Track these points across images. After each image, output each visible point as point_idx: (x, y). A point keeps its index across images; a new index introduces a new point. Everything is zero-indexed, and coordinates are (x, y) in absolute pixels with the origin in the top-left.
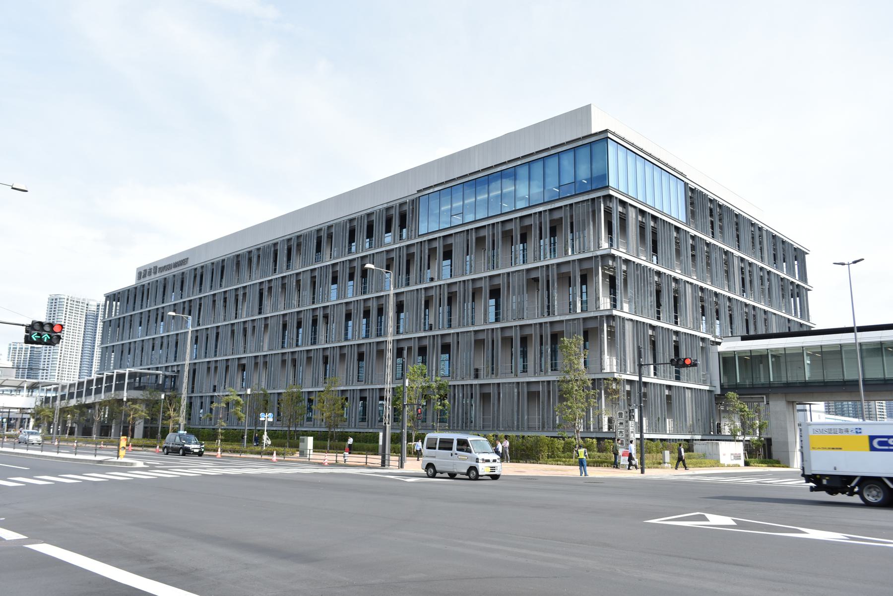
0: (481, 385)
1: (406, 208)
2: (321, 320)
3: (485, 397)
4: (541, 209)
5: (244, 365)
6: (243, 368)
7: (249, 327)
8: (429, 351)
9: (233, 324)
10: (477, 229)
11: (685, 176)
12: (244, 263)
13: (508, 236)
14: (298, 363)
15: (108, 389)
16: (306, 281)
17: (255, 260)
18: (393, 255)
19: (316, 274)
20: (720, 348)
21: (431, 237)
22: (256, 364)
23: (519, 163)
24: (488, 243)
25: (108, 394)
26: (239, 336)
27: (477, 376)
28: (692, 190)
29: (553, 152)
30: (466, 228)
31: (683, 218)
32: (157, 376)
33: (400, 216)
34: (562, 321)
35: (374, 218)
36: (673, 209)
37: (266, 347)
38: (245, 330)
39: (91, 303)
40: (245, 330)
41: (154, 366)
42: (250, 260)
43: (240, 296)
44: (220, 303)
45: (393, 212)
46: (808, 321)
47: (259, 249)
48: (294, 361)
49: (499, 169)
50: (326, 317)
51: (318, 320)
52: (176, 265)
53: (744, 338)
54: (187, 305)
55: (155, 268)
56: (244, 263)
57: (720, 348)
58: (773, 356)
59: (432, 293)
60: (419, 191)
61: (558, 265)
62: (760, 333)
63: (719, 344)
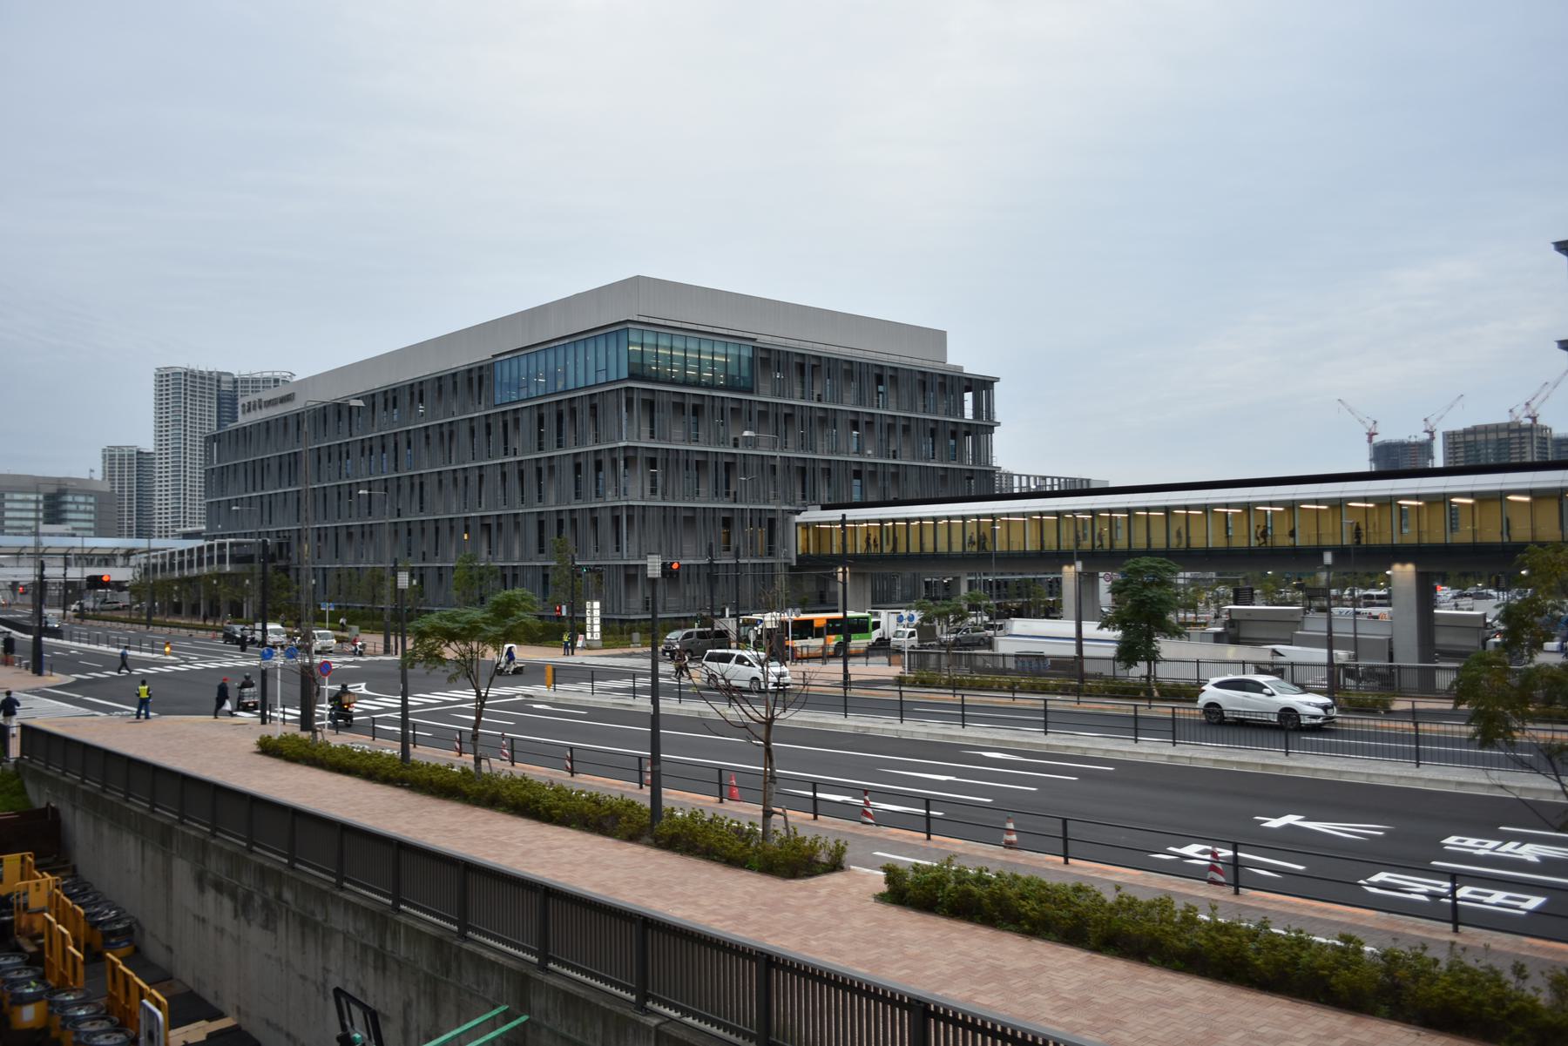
33: (476, 379)
39: (224, 378)
53: (825, 508)
57: (798, 519)
63: (798, 512)
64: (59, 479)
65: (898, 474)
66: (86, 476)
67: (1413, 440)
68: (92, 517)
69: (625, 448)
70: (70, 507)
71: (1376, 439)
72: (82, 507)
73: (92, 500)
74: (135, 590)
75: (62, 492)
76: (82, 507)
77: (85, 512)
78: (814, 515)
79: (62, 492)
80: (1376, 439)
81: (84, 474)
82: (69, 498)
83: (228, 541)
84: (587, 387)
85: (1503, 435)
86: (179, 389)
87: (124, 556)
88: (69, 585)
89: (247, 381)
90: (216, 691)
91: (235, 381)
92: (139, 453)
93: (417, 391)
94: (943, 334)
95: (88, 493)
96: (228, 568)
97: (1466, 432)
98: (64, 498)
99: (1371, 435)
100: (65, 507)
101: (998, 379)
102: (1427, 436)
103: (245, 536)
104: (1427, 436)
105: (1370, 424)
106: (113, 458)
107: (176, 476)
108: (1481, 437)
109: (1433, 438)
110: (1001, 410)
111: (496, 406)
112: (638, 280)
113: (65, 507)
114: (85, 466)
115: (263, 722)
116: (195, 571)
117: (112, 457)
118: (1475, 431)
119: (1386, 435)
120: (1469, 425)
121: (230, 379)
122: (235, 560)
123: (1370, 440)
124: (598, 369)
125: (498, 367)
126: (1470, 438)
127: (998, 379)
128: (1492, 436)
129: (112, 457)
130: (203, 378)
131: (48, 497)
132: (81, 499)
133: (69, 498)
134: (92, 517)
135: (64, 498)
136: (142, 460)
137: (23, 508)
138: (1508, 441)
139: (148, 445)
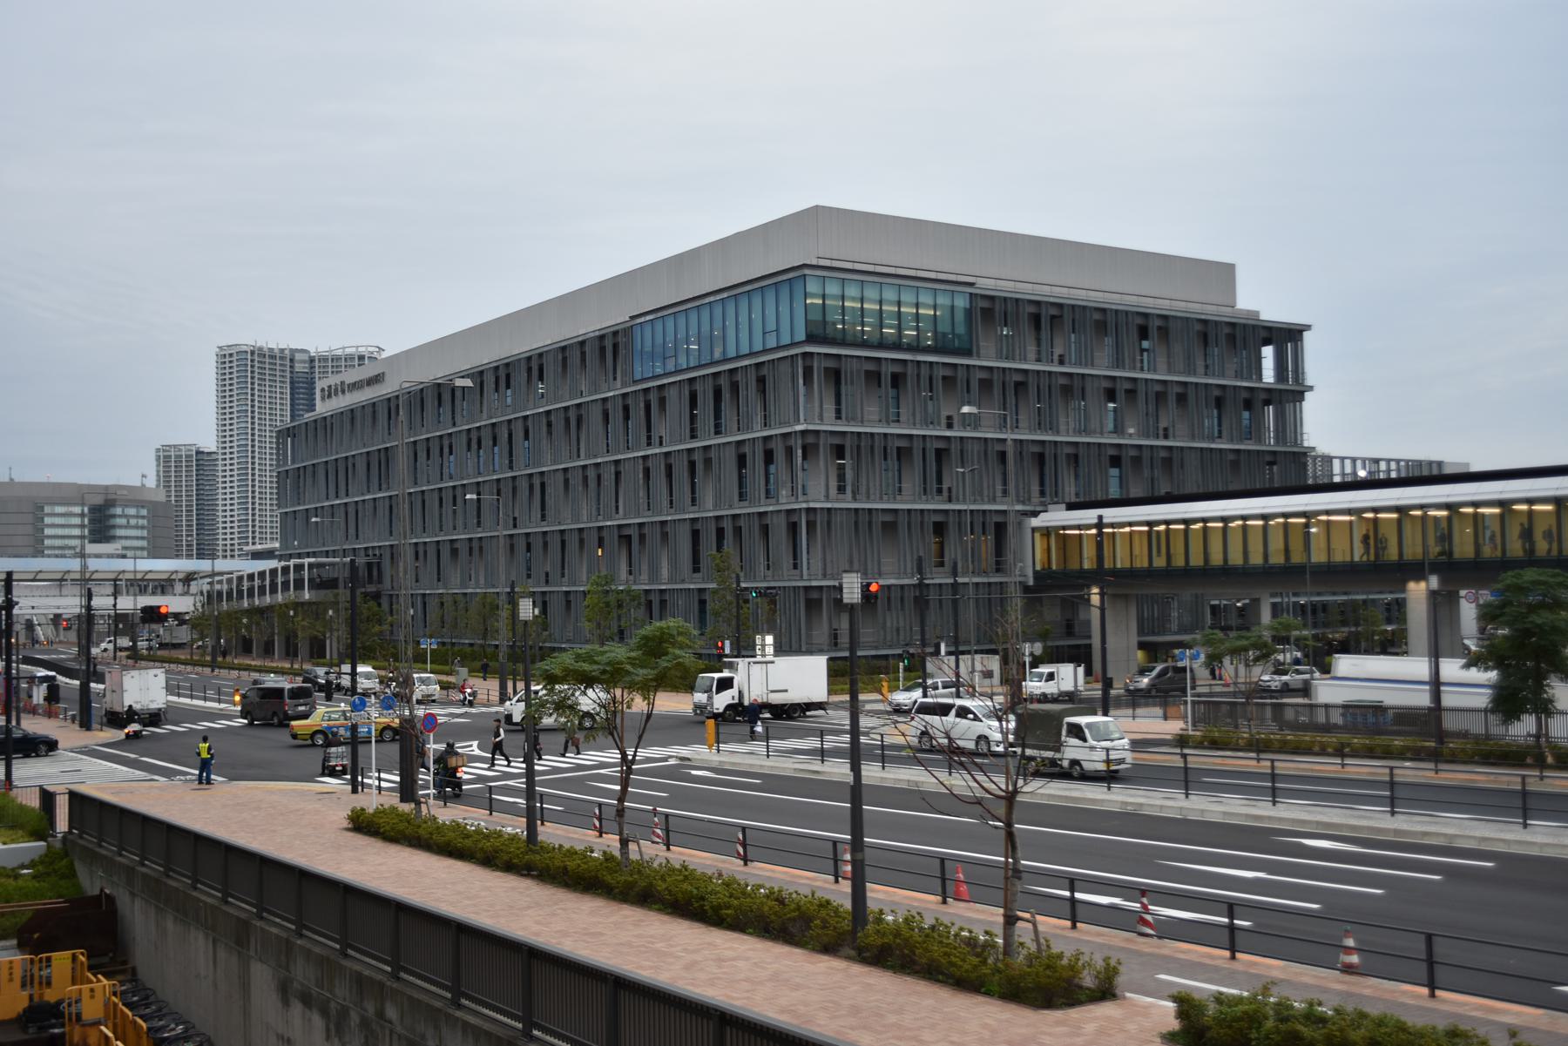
29: (756, 285)
33: (609, 349)
38: (692, 464)
39: (298, 356)
40: (692, 464)
49: (707, 300)
60: (632, 318)
63: (1035, 514)
69: (803, 432)
70: (120, 521)
72: (133, 522)
73: (144, 512)
76: (133, 522)
77: (137, 527)
78: (1057, 517)
82: (119, 511)
83: (306, 561)
84: (752, 354)
86: (245, 370)
91: (312, 360)
92: (198, 453)
95: (140, 504)
101: (1308, 327)
106: (169, 460)
111: (635, 382)
112: (817, 212)
117: (167, 458)
122: (314, 585)
124: (771, 329)
127: (1308, 327)
129: (167, 458)
131: (95, 510)
132: (132, 511)
133: (119, 511)
139: (209, 443)
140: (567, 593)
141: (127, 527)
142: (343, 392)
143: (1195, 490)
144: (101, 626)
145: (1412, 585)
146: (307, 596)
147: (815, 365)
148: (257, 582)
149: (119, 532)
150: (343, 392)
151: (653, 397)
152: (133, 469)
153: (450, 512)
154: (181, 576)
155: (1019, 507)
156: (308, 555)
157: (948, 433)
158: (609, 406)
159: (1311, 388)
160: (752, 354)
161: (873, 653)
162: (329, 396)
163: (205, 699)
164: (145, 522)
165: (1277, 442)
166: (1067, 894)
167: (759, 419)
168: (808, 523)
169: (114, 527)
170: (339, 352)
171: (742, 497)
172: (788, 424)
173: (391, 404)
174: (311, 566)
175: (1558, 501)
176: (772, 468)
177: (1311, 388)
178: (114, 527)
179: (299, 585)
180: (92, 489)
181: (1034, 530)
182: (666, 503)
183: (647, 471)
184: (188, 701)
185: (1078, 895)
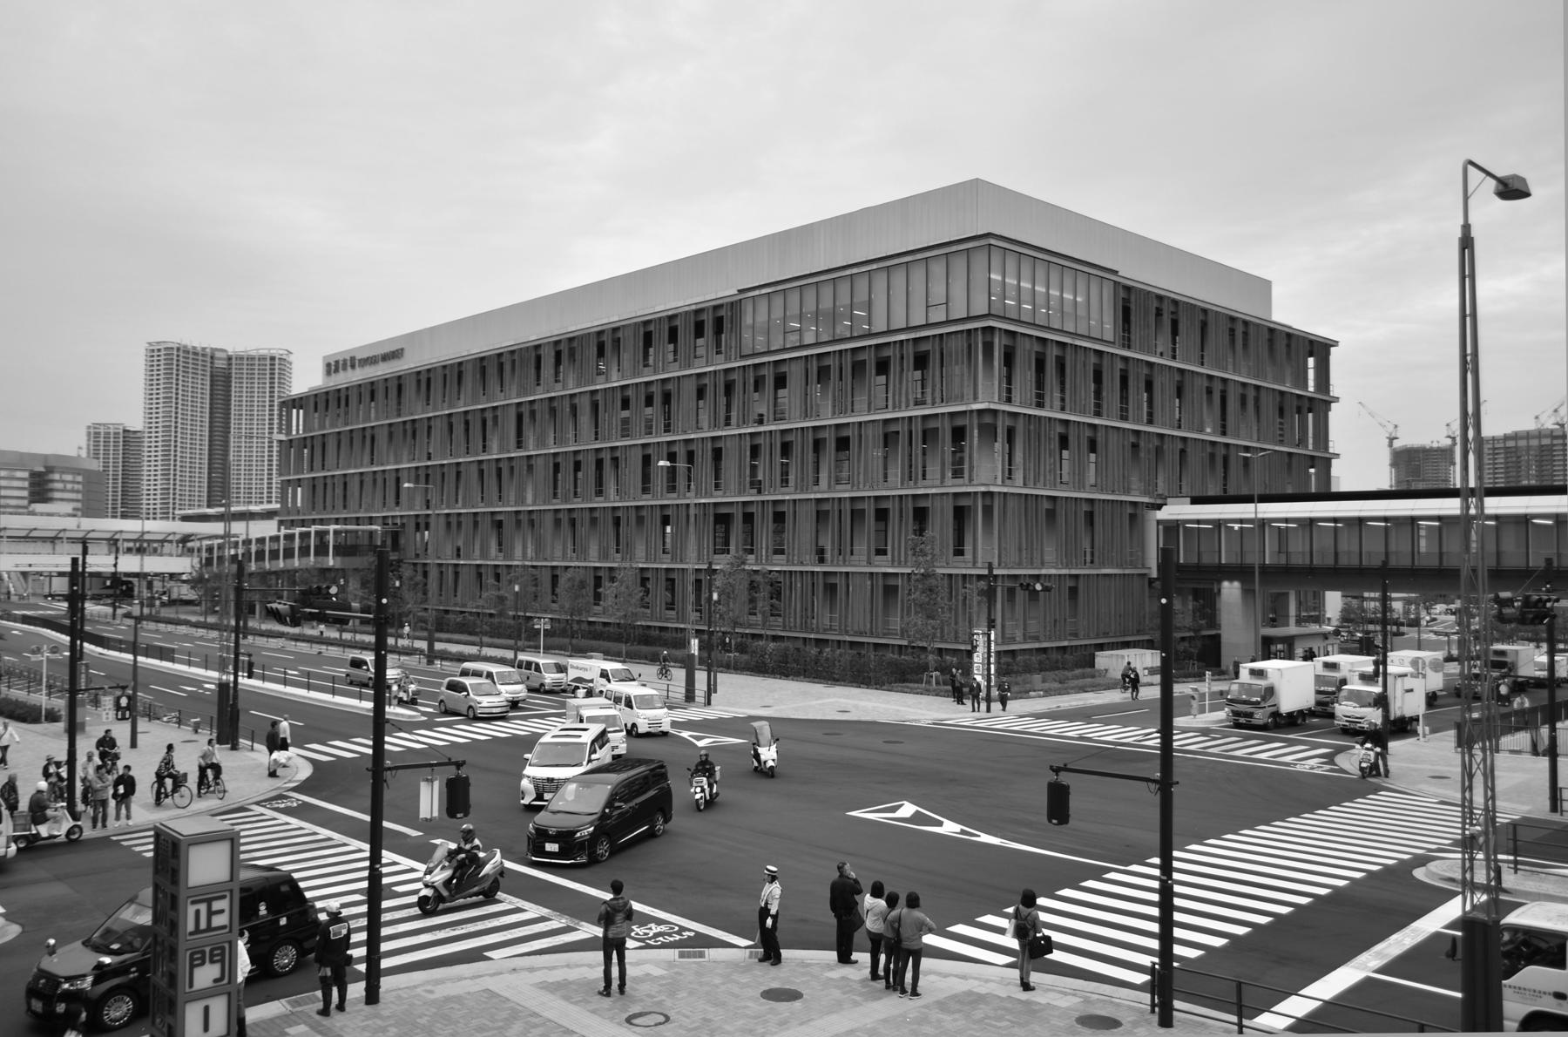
0: (825, 573)
1: (722, 313)
2: (607, 464)
3: (831, 589)
4: (903, 337)
5: (501, 522)
6: (499, 525)
7: (505, 467)
8: (757, 520)
9: (480, 462)
10: (819, 355)
11: (1115, 272)
12: (492, 371)
13: (858, 368)
14: (578, 523)
15: (304, 551)
16: (585, 405)
17: (507, 367)
18: (706, 381)
19: (599, 397)
20: (1162, 514)
21: (757, 361)
22: (518, 523)
23: (875, 266)
24: (834, 374)
25: (304, 560)
26: (491, 481)
27: (822, 561)
28: (1128, 289)
29: (919, 256)
30: (805, 353)
31: (1109, 330)
32: (371, 533)
33: (714, 322)
34: (927, 495)
35: (678, 322)
36: (1093, 322)
37: (529, 499)
38: (499, 471)
39: (218, 355)
40: (499, 471)
41: (372, 518)
42: (501, 366)
43: (485, 422)
44: (459, 429)
45: (704, 317)
46: (1326, 448)
47: (512, 352)
48: (573, 523)
49: (848, 272)
50: (615, 460)
51: (603, 466)
52: (386, 357)
53: (1196, 501)
54: (408, 426)
55: (353, 359)
56: (492, 371)
57: (1162, 514)
58: (975, 693)
59: (760, 441)
60: (740, 291)
61: (925, 417)
62: (1231, 492)
63: (1159, 507)
64: (46, 457)
65: (1220, 458)
66: (73, 453)
67: (1435, 445)
68: (80, 496)
69: (980, 412)
70: (59, 486)
71: (1397, 444)
72: (69, 486)
73: (79, 478)
74: (196, 582)
75: (50, 470)
76: (69, 486)
77: (72, 491)
78: (1179, 510)
79: (50, 470)
80: (1397, 444)
81: (71, 452)
82: (57, 476)
83: (332, 527)
84: (908, 329)
85: (1546, 441)
86: (173, 364)
87: (161, 542)
88: (116, 578)
89: (253, 358)
90: (460, 759)
91: (230, 358)
92: (125, 431)
93: (605, 343)
94: (1266, 285)
95: (76, 472)
96: (331, 561)
97: (1506, 438)
98: (51, 477)
99: (1391, 440)
100: (51, 485)
101: (1335, 343)
102: (1449, 442)
103: (358, 521)
104: (1449, 442)
105: (1391, 428)
106: (98, 437)
107: (166, 455)
108: (1522, 443)
109: (1454, 444)
110: (1339, 383)
111: (743, 357)
112: (976, 184)
113: (51, 485)
114: (69, 442)
115: (1241, 1032)
116: (281, 564)
117: (97, 434)
118: (1516, 436)
119: (1406, 440)
120: (1509, 430)
121: (223, 355)
122: (340, 550)
123: (1391, 445)
124: (952, 299)
125: (748, 308)
126: (1511, 444)
127: (1335, 343)
128: (1534, 443)
129: (97, 434)
130: (196, 354)
131: (33, 475)
132: (69, 477)
133: (57, 476)
134: (80, 496)
135: (51, 477)
136: (129, 439)
137: (19, 487)
138: (1550, 448)
139: (136, 422)
140: (479, 566)
141: (64, 490)
142: (353, 367)
143: (1290, 491)
144: (91, 588)
145: (1226, 584)
146: (331, 563)
147: (997, 341)
148: (253, 548)
149: (57, 495)
150: (353, 367)
151: (489, 415)
152: (66, 440)
153: (920, 452)
154: (178, 537)
155: (1146, 500)
156: (314, 522)
157: (1096, 421)
158: (453, 420)
159: (1337, 399)
160: (908, 329)
161: (1037, 645)
162: (336, 371)
163: (285, 682)
164: (80, 487)
165: (1316, 447)
166: (140, 659)
167: (571, 435)
168: (984, 507)
169: (52, 490)
170: (253, 353)
171: (645, 490)
172: (961, 398)
173: (399, 382)
174: (336, 532)
175: (1559, 518)
176: (580, 475)
177: (1337, 399)
178: (52, 490)
179: (322, 550)
180: (34, 457)
181: (1159, 522)
182: (496, 498)
183: (481, 472)
184: (303, 692)
185: (131, 657)
